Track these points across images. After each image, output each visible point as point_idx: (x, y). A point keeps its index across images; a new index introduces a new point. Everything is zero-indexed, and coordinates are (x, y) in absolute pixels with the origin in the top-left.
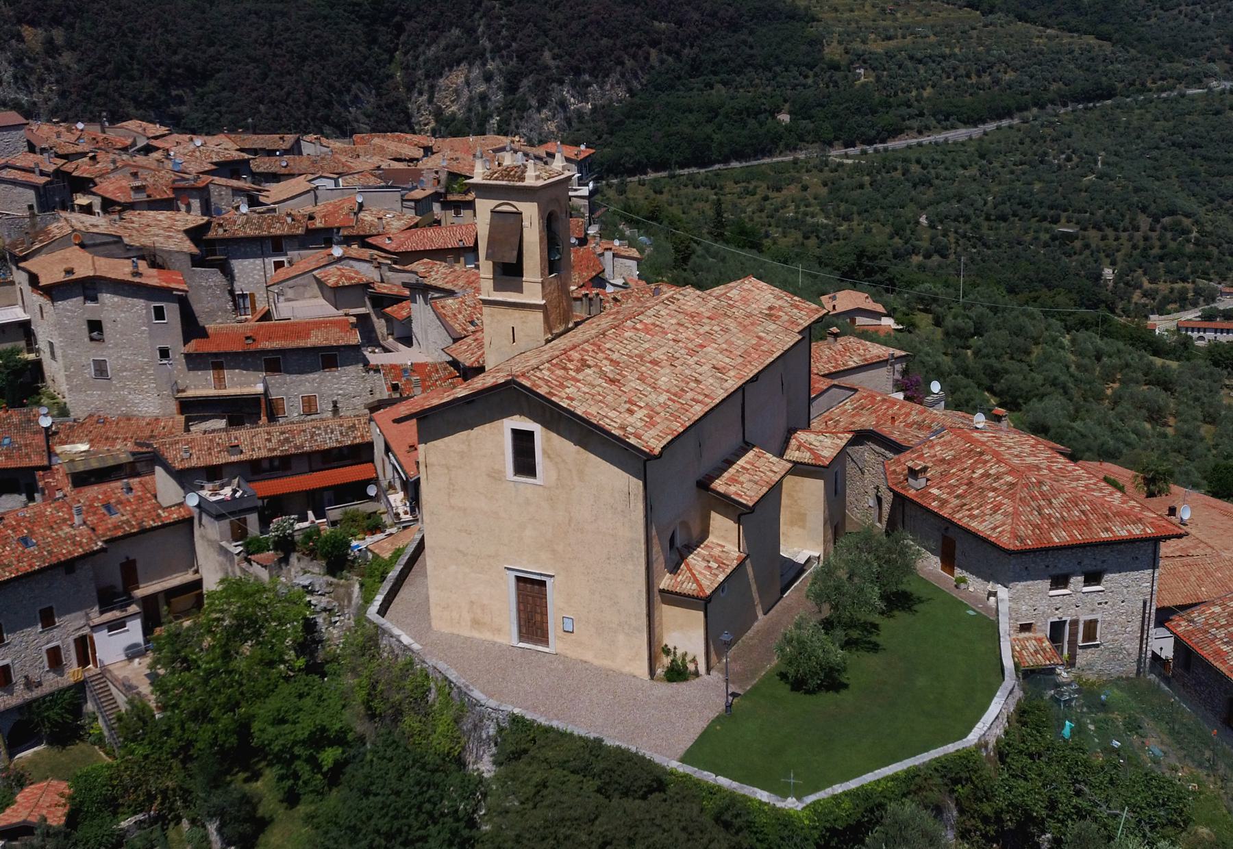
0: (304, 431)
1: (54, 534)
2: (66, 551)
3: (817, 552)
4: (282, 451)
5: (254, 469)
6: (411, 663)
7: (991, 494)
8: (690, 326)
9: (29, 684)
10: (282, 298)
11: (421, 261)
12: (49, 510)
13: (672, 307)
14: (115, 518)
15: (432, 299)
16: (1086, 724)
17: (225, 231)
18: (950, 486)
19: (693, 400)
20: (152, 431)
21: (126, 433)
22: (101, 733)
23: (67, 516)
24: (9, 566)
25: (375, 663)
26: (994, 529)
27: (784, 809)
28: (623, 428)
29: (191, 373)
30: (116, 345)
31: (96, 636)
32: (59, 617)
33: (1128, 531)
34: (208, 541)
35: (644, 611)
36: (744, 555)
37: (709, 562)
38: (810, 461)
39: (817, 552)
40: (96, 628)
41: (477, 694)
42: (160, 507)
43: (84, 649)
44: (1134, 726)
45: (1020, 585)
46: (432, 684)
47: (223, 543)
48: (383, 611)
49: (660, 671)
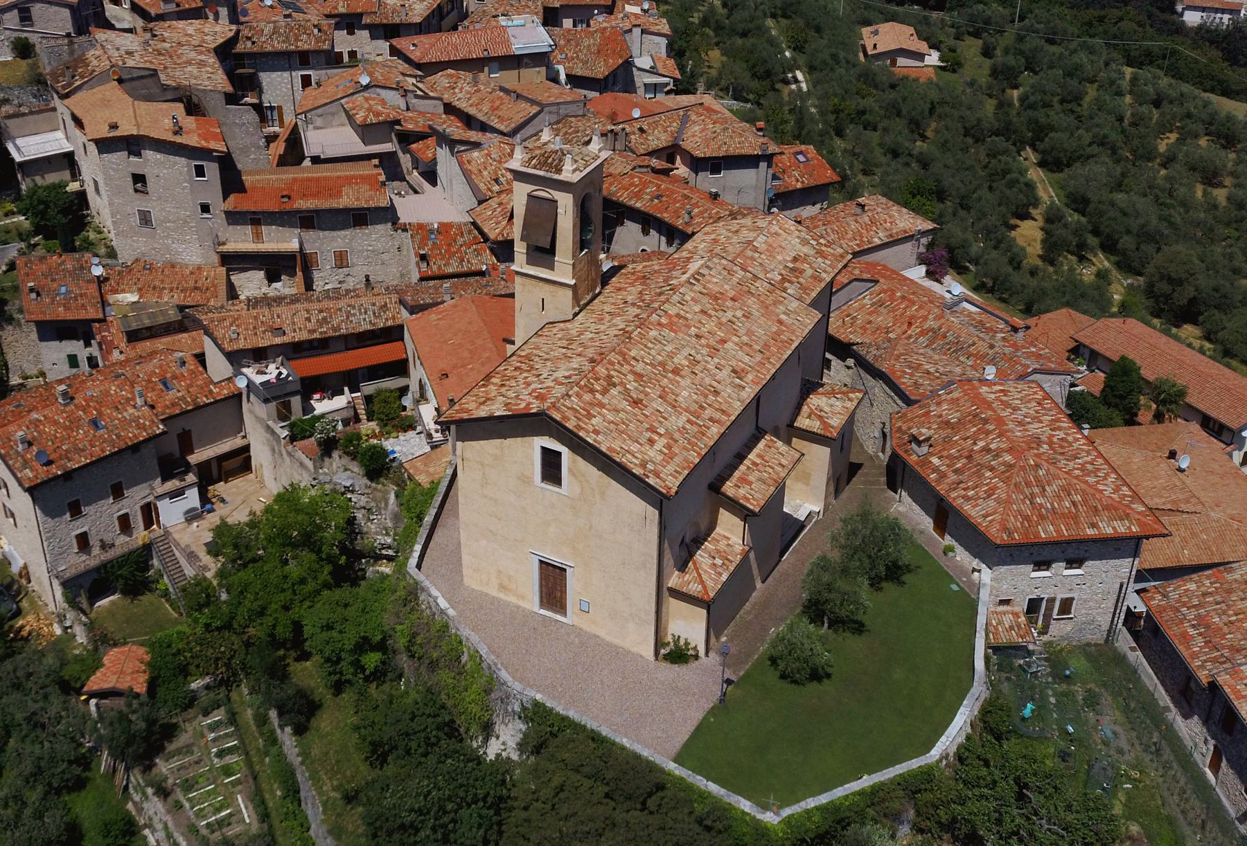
0: (340, 310)
1: (120, 416)
2: (134, 435)
3: (817, 507)
4: (321, 333)
5: (294, 351)
6: (446, 626)
7: (988, 474)
8: (713, 313)
9: (104, 546)
10: (311, 127)
11: (445, 72)
12: (113, 388)
13: (698, 287)
14: (172, 395)
15: (458, 152)
16: (1048, 696)
17: (254, 43)
18: (949, 457)
19: (711, 419)
20: (196, 282)
21: (172, 283)
22: (167, 589)
23: (129, 396)
24: (83, 450)
25: (414, 617)
26: (985, 516)
27: (762, 821)
28: (643, 465)
29: (231, 227)
30: (160, 198)
31: (159, 504)
32: (127, 489)
33: (1114, 528)
34: (257, 417)
35: (654, 610)
36: (747, 548)
37: (714, 558)
38: (819, 432)
39: (817, 507)
40: (160, 497)
41: (504, 675)
42: (212, 382)
43: (149, 514)
44: (1092, 701)
45: (1004, 569)
46: (465, 649)
47: (270, 423)
48: (419, 566)
49: (660, 656)
